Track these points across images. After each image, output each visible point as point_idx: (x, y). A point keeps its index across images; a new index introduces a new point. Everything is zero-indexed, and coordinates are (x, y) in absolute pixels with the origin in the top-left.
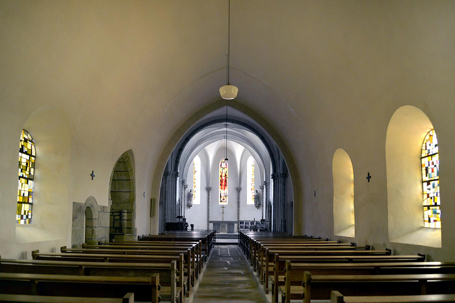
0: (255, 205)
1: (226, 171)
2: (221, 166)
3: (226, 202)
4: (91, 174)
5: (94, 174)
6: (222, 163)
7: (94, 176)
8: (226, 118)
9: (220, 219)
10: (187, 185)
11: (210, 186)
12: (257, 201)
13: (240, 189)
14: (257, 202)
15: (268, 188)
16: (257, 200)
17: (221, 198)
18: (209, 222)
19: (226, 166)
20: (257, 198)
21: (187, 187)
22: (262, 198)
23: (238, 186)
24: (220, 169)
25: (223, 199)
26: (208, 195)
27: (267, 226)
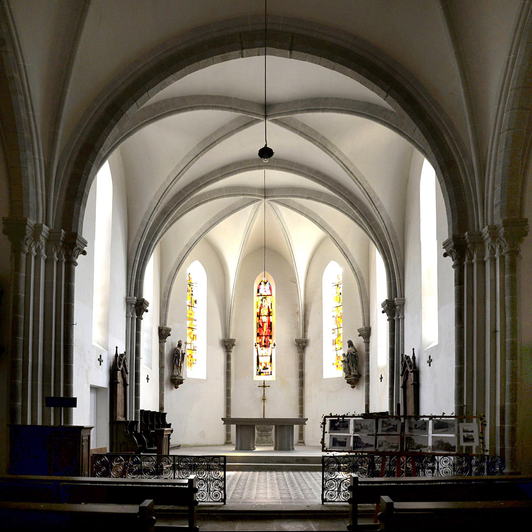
0: (346, 378)
1: (271, 304)
2: (258, 292)
3: (271, 374)
4: (99, 359)
5: (102, 359)
6: (260, 284)
7: (102, 362)
8: (263, 27)
9: (256, 415)
10: (170, 330)
11: (231, 337)
12: (351, 367)
13: (306, 342)
14: (350, 370)
15: (399, 320)
16: (352, 366)
17: (260, 365)
18: (228, 421)
19: (271, 292)
20: (352, 361)
21: (169, 335)
22: (364, 360)
23: (301, 337)
24: (257, 300)
25: (265, 368)
26: (226, 359)
27: (466, 440)
